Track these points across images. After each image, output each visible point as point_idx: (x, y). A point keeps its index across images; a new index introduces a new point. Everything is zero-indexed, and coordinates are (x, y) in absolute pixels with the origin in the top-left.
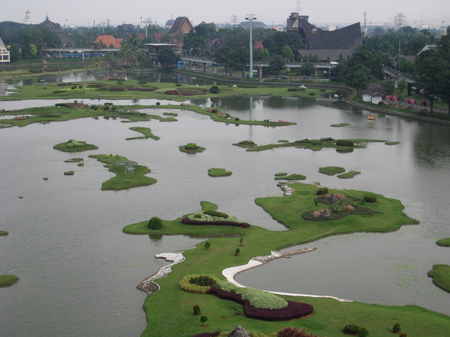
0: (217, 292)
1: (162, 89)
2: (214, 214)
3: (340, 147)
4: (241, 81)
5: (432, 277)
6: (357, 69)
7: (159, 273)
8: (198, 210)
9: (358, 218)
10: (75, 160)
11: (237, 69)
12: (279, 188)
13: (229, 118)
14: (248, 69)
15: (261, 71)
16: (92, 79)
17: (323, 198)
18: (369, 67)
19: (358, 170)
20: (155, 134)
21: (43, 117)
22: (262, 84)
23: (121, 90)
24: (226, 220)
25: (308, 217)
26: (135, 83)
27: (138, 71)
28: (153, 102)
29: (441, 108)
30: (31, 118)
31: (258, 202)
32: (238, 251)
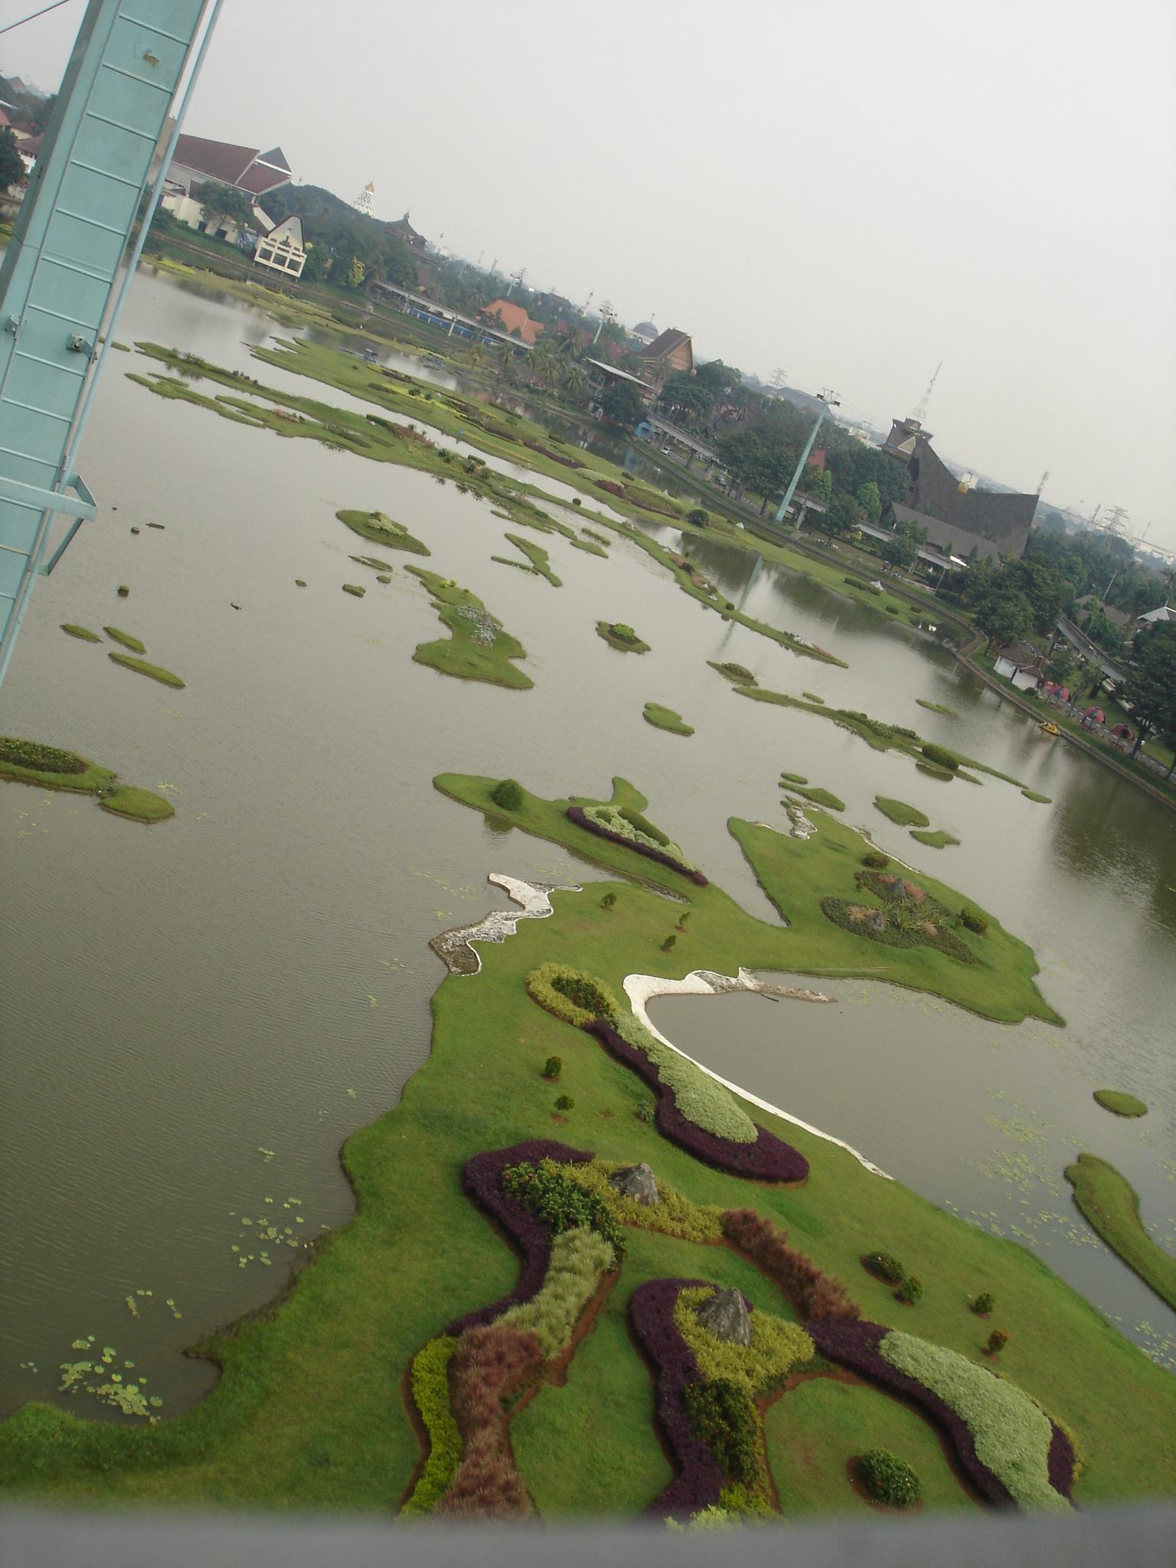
0: (605, 1034)
1: (595, 473)
2: (640, 825)
3: (928, 761)
4: (754, 519)
5: (1074, 1184)
6: (1009, 599)
7: (487, 924)
8: (602, 792)
9: (939, 959)
10: (375, 564)
11: (756, 490)
12: (784, 810)
13: (713, 597)
14: (778, 500)
15: (802, 514)
16: (451, 385)
17: (875, 877)
18: (1032, 603)
19: (956, 837)
20: (555, 570)
21: (333, 432)
22: (795, 543)
23: (510, 438)
24: (662, 849)
25: (834, 913)
26: (539, 432)
27: (552, 408)
28: (568, 493)
29: (1155, 755)
30: (308, 424)
31: (736, 828)
32: (671, 941)
